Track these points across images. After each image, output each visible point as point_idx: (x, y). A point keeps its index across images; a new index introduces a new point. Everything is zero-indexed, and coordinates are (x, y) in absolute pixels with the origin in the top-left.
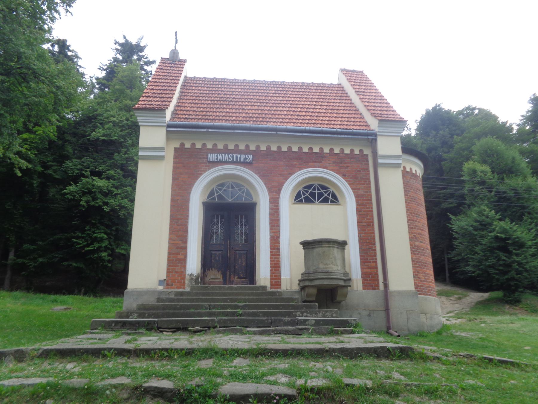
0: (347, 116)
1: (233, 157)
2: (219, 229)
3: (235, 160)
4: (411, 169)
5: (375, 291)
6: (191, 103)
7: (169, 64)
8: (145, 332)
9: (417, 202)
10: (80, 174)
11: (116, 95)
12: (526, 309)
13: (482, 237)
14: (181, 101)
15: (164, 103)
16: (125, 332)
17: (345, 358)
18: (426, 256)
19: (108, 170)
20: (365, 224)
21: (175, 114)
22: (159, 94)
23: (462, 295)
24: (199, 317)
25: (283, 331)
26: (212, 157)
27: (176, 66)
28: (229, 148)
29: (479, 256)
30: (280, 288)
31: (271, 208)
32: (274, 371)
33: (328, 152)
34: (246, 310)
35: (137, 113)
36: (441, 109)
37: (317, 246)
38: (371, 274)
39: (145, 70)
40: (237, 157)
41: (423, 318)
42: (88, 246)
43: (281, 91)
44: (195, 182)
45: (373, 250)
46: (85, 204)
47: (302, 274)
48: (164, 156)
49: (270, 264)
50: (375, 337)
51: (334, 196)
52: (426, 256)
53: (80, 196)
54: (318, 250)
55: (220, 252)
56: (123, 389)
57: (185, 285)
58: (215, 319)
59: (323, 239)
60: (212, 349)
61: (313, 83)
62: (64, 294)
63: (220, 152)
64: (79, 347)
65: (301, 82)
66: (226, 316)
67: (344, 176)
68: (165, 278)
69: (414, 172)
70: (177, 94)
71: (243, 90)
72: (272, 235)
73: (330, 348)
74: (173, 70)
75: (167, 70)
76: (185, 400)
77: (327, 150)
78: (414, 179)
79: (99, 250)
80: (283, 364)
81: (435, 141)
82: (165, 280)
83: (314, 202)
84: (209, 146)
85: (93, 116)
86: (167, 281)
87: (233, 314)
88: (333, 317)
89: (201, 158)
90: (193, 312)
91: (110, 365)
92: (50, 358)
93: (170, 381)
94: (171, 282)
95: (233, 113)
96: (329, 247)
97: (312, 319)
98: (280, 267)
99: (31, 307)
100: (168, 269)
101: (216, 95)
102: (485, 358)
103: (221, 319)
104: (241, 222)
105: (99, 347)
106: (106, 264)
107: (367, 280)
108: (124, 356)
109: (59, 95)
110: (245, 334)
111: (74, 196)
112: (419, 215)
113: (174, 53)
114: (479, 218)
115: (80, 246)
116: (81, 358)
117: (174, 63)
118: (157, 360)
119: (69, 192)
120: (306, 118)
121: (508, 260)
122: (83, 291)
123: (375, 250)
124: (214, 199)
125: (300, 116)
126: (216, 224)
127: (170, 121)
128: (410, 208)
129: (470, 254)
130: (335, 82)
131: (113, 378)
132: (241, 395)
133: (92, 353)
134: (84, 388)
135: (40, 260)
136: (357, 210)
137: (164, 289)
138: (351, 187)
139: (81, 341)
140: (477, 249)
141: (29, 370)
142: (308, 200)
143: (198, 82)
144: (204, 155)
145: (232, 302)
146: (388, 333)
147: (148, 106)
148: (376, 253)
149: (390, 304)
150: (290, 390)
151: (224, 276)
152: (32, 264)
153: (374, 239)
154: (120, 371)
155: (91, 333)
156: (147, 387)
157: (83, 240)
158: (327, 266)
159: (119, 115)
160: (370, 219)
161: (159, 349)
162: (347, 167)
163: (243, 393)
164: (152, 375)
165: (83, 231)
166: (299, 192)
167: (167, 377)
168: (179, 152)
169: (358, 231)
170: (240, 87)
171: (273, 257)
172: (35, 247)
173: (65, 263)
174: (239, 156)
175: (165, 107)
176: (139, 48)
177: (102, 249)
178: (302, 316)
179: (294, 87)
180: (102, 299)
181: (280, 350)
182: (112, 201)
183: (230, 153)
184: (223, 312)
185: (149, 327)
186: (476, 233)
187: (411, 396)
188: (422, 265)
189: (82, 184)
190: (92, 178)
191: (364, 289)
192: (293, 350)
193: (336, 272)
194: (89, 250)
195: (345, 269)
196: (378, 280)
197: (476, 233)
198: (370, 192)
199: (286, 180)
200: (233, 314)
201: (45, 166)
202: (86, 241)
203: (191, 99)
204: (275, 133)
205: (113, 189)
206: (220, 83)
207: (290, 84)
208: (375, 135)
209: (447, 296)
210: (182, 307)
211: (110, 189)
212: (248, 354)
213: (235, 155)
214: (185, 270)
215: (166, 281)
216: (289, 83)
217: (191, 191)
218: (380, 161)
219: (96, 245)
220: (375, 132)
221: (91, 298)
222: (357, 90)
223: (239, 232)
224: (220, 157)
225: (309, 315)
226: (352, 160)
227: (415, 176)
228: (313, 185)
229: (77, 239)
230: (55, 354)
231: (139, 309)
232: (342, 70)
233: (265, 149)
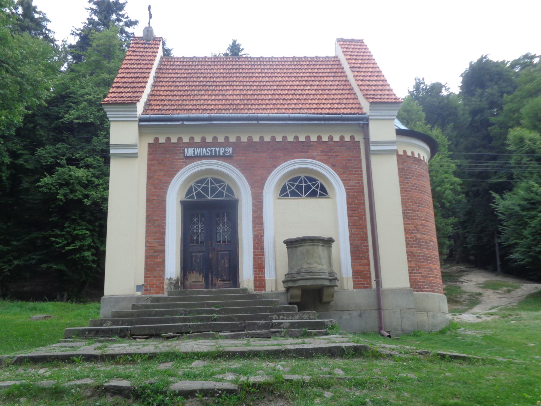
0: (339, 97)
1: (211, 151)
2: (199, 228)
3: (213, 154)
4: (412, 153)
5: (367, 289)
6: (167, 91)
7: (142, 44)
8: (117, 339)
9: (419, 190)
10: (55, 163)
11: (91, 68)
13: (533, 218)
14: (156, 88)
15: (135, 95)
16: (98, 340)
17: (300, 358)
18: (430, 249)
19: (87, 157)
20: (356, 218)
21: (148, 104)
22: (131, 83)
23: (512, 287)
24: (173, 323)
25: (255, 334)
26: (189, 152)
27: (150, 46)
28: (207, 141)
29: (528, 241)
30: (265, 290)
31: (253, 205)
32: (223, 372)
34: (223, 314)
35: (106, 108)
36: (489, 62)
37: (301, 245)
38: (363, 271)
39: (126, 33)
40: (215, 150)
41: (423, 317)
42: (68, 245)
43: (268, 69)
44: (171, 180)
46: (62, 198)
48: (137, 153)
49: (254, 265)
50: (343, 337)
51: (323, 189)
52: (430, 249)
53: (57, 189)
54: (301, 249)
55: (201, 254)
56: (86, 388)
58: (188, 325)
60: (173, 353)
61: (305, 57)
62: (44, 301)
63: (198, 145)
64: (50, 354)
65: (292, 56)
66: (200, 321)
67: (333, 166)
69: (416, 156)
70: (151, 81)
71: (225, 71)
73: (286, 350)
74: (147, 52)
75: (140, 52)
76: (140, 396)
77: (314, 138)
78: (417, 164)
79: (81, 249)
80: (235, 364)
81: (480, 101)
82: (143, 285)
83: (301, 196)
84: (186, 140)
85: (66, 93)
86: (145, 287)
87: (208, 319)
88: (311, 319)
89: (177, 154)
90: (167, 318)
91: (78, 369)
92: (24, 365)
93: (129, 380)
94: (150, 287)
95: (246, 65)
96: (313, 245)
97: (287, 321)
99: (7, 317)
100: (146, 274)
101: (195, 79)
102: (438, 354)
103: (195, 325)
104: (223, 220)
105: (68, 354)
106: (91, 265)
107: (358, 278)
108: (92, 361)
109: (24, 85)
110: (217, 339)
111: (50, 189)
112: (422, 204)
114: (526, 196)
115: (59, 245)
116: (51, 364)
117: (148, 43)
118: (122, 364)
119: (43, 184)
120: (292, 102)
122: (66, 296)
123: (367, 246)
125: (286, 100)
127: (142, 114)
128: (412, 197)
129: (518, 239)
130: (332, 54)
131: (79, 380)
132: (188, 391)
133: (62, 359)
134: (52, 388)
135: (16, 262)
136: (347, 203)
137: (142, 294)
138: (340, 178)
139: (54, 349)
140: (526, 232)
141: (5, 375)
142: (294, 195)
143: (175, 63)
145: (209, 307)
146: (379, 333)
147: (118, 99)
148: (368, 249)
149: (382, 303)
150: (233, 385)
151: (206, 278)
152: (7, 267)
153: (366, 233)
154: (85, 374)
155: (65, 342)
156: (107, 386)
157: (63, 238)
158: (311, 266)
159: (96, 91)
160: (361, 212)
161: (124, 355)
163: (190, 389)
164: (114, 376)
165: (62, 228)
166: (285, 186)
167: (127, 377)
168: (153, 148)
169: (349, 225)
170: (222, 67)
172: (9, 248)
173: (44, 266)
174: (217, 150)
175: (137, 99)
176: (118, 6)
177: (84, 248)
178: (278, 319)
179: (283, 63)
180: (85, 305)
181: (238, 352)
182: (93, 193)
183: (209, 147)
184: (197, 317)
185: (122, 334)
186: (524, 213)
187: (342, 387)
188: (425, 260)
189: (57, 175)
190: (68, 167)
191: (354, 288)
192: (250, 352)
193: (320, 271)
194: (70, 250)
196: (370, 277)
197: (524, 213)
198: (362, 183)
199: (270, 173)
200: (208, 319)
201: (14, 155)
202: (66, 239)
203: (166, 86)
204: (256, 122)
205: (93, 179)
206: (200, 63)
207: (279, 59)
209: (494, 289)
210: (157, 314)
211: (90, 179)
212: (207, 357)
213: (213, 149)
215: (144, 287)
216: (278, 58)
217: (167, 189)
218: (372, 148)
219: (78, 244)
221: (74, 304)
222: (353, 65)
223: (221, 231)
224: (197, 151)
225: (285, 318)
226: (342, 148)
227: (418, 160)
229: (56, 238)
230: (28, 361)
231: (114, 317)
232: (339, 40)
233: (246, 140)
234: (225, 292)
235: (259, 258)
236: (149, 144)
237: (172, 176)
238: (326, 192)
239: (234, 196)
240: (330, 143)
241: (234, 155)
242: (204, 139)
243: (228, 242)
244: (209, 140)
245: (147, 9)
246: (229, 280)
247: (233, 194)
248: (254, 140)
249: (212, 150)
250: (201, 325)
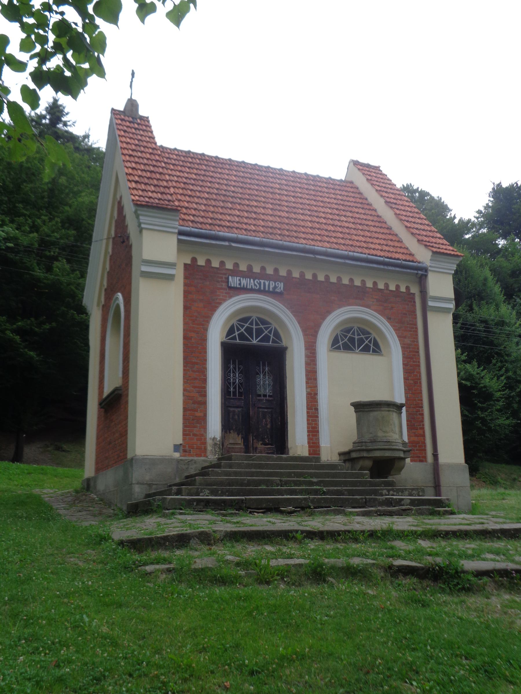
1: (260, 284)
2: (237, 378)
3: (262, 288)
12: (484, 480)
25: (387, 512)
26: (234, 281)
31: (307, 356)
33: (371, 286)
38: (418, 443)
47: (354, 443)
49: (308, 428)
51: (376, 344)
55: (240, 409)
57: (206, 453)
59: (382, 401)
63: (243, 274)
67: (389, 319)
68: (181, 443)
72: (309, 390)
82: (181, 444)
84: (229, 266)
86: (184, 446)
89: (218, 282)
94: (189, 447)
96: (389, 411)
98: (318, 432)
100: (184, 431)
104: (264, 370)
113: (132, 104)
123: (422, 414)
126: (233, 372)
136: (403, 364)
137: (181, 456)
138: (396, 333)
144: (222, 278)
148: (423, 418)
151: (246, 440)
153: (422, 400)
162: (392, 308)
171: (310, 419)
174: (267, 283)
178: (388, 495)
195: (402, 438)
196: (425, 450)
198: (417, 342)
199: (324, 319)
208: (426, 270)
210: (249, 483)
213: (262, 281)
214: (206, 433)
217: (208, 326)
218: (430, 303)
220: (424, 265)
224: (244, 282)
225: (395, 493)
228: (369, 333)
234: (268, 459)
235: (313, 421)
236: (185, 265)
237: (214, 309)
239: (282, 342)
242: (250, 268)
243: (270, 396)
244: (256, 269)
245: (135, 75)
246: (272, 445)
249: (260, 282)
250: (321, 498)
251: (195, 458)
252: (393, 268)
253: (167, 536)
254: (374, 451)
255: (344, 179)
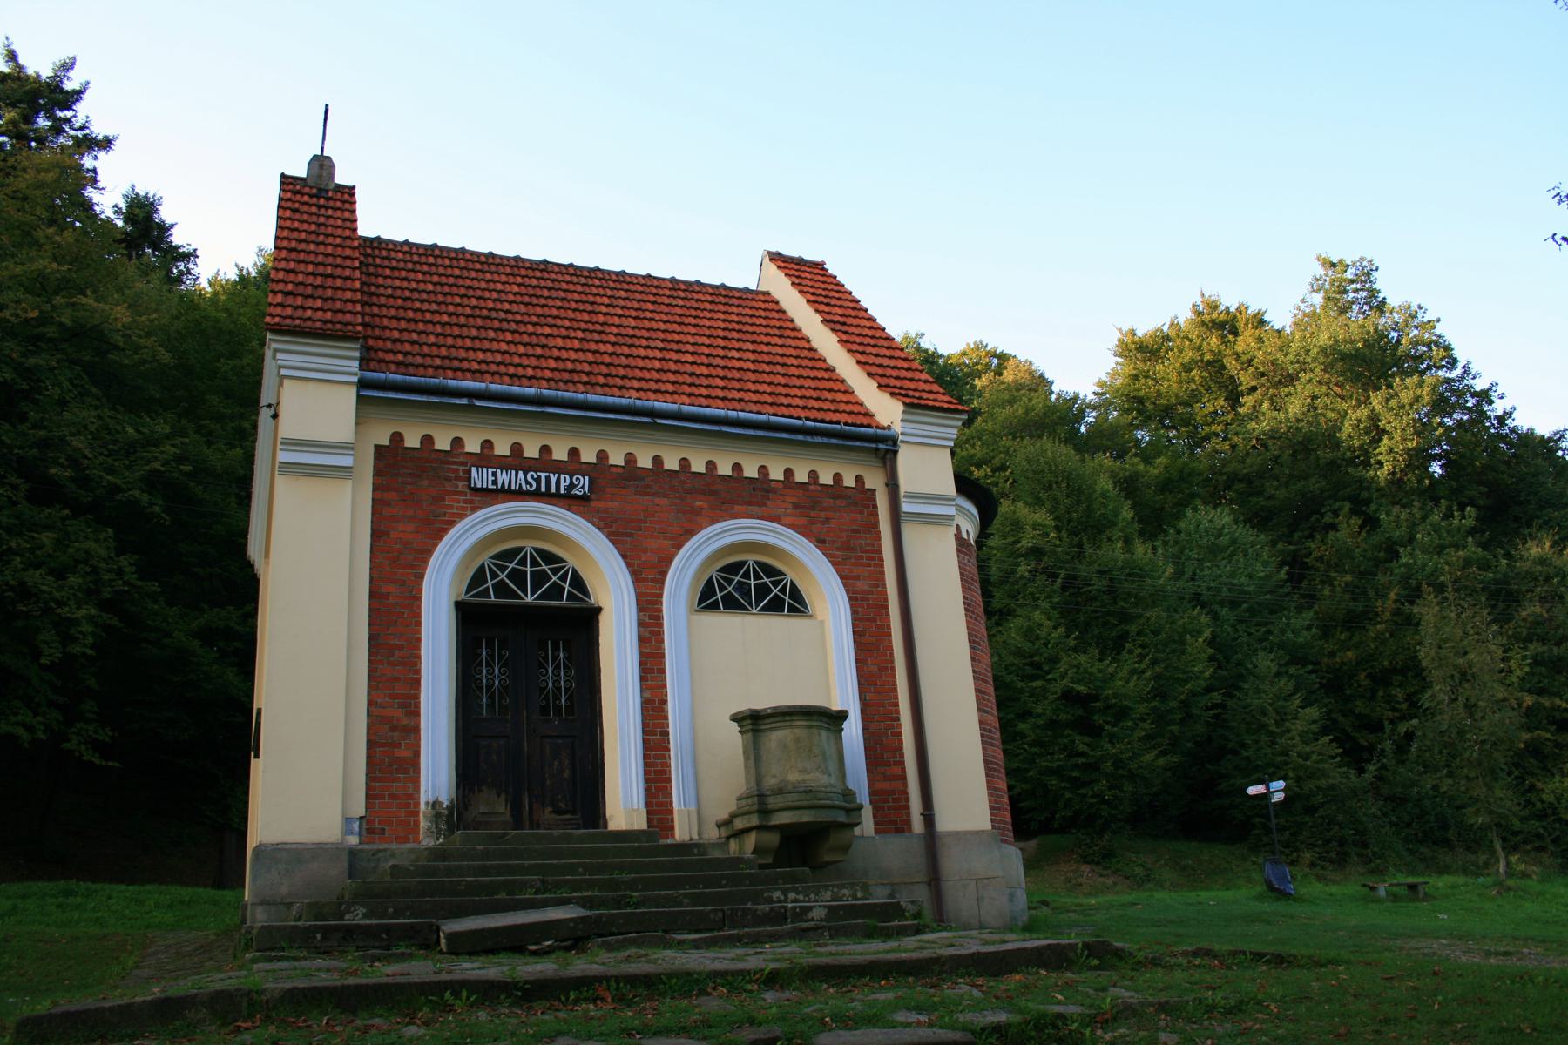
1: (538, 480)
2: (493, 675)
3: (543, 489)
30: (673, 836)
31: (641, 624)
38: (892, 792)
40: (548, 480)
44: (435, 546)
45: (894, 734)
47: (739, 799)
51: (796, 594)
63: (503, 464)
67: (820, 543)
72: (647, 695)
77: (777, 474)
96: (810, 727)
104: (555, 658)
113: (322, 164)
121: (1091, 753)
124: (486, 593)
126: (488, 665)
142: (732, 605)
144: (457, 471)
153: (897, 705)
162: (828, 519)
168: (390, 459)
174: (553, 479)
191: (877, 831)
196: (907, 807)
198: (884, 586)
199: (679, 547)
208: (894, 441)
213: (543, 475)
218: (906, 507)
224: (503, 477)
225: (801, 897)
236: (378, 448)
237: (439, 534)
238: (802, 601)
240: (812, 487)
241: (593, 496)
244: (531, 451)
246: (573, 812)
247: (586, 593)
248: (640, 464)
249: (539, 477)
251: (394, 846)
252: (825, 440)
253: (129, 1006)
254: (779, 813)
255: (753, 287)
